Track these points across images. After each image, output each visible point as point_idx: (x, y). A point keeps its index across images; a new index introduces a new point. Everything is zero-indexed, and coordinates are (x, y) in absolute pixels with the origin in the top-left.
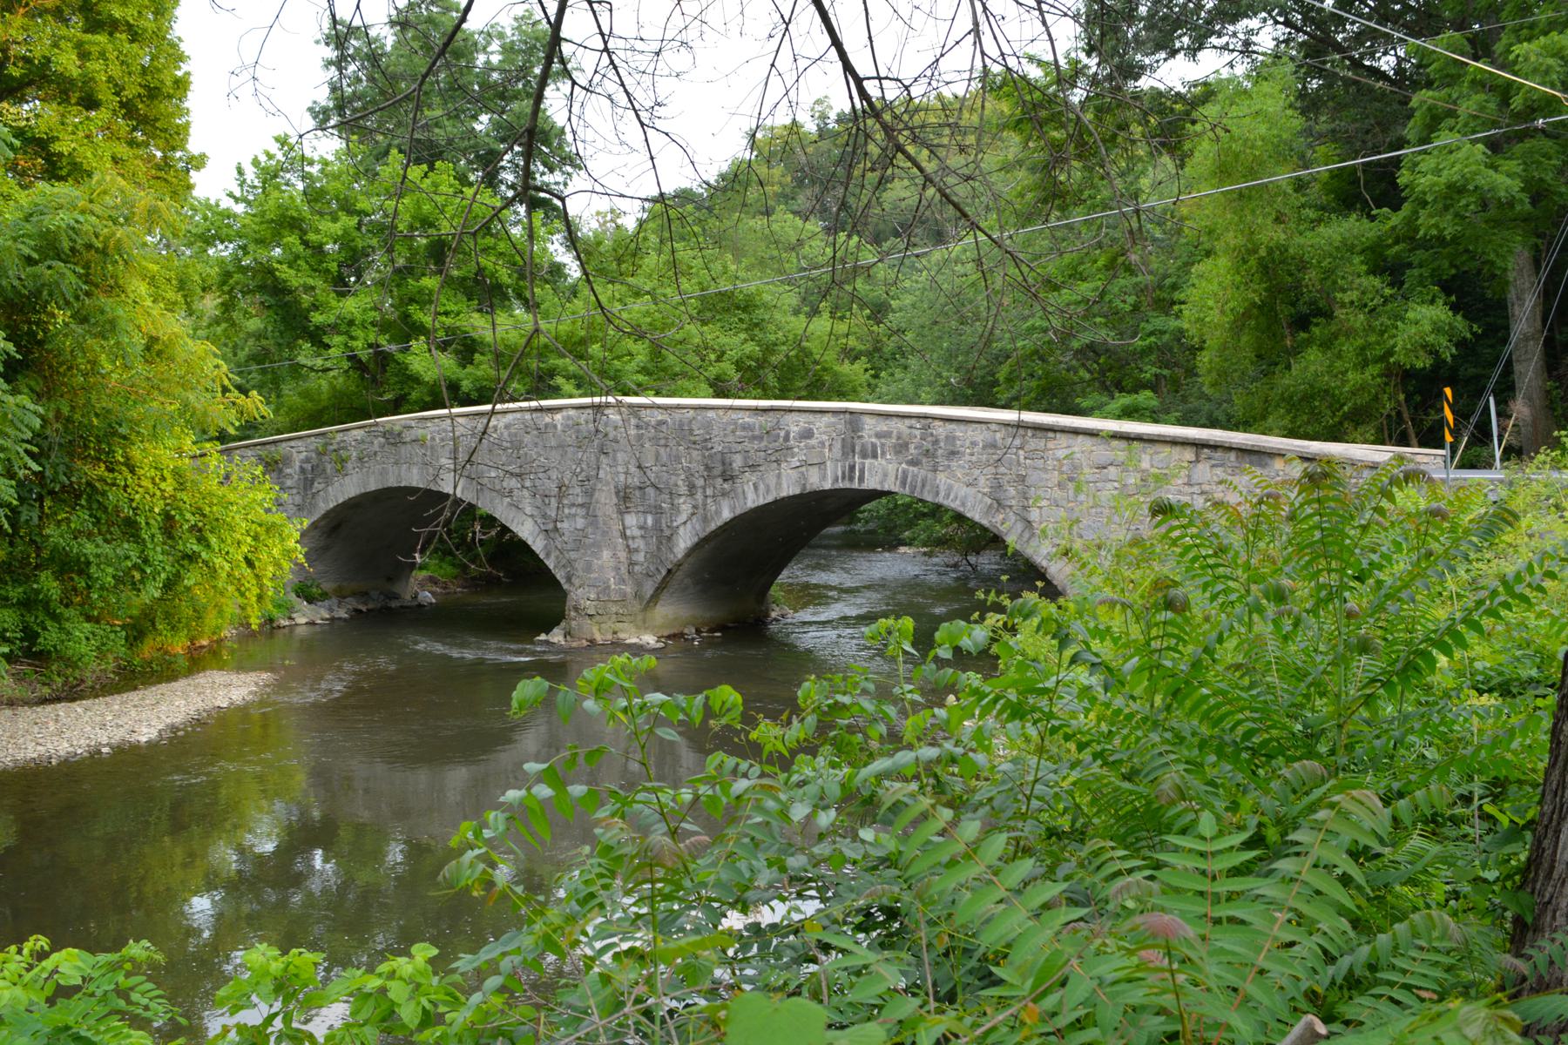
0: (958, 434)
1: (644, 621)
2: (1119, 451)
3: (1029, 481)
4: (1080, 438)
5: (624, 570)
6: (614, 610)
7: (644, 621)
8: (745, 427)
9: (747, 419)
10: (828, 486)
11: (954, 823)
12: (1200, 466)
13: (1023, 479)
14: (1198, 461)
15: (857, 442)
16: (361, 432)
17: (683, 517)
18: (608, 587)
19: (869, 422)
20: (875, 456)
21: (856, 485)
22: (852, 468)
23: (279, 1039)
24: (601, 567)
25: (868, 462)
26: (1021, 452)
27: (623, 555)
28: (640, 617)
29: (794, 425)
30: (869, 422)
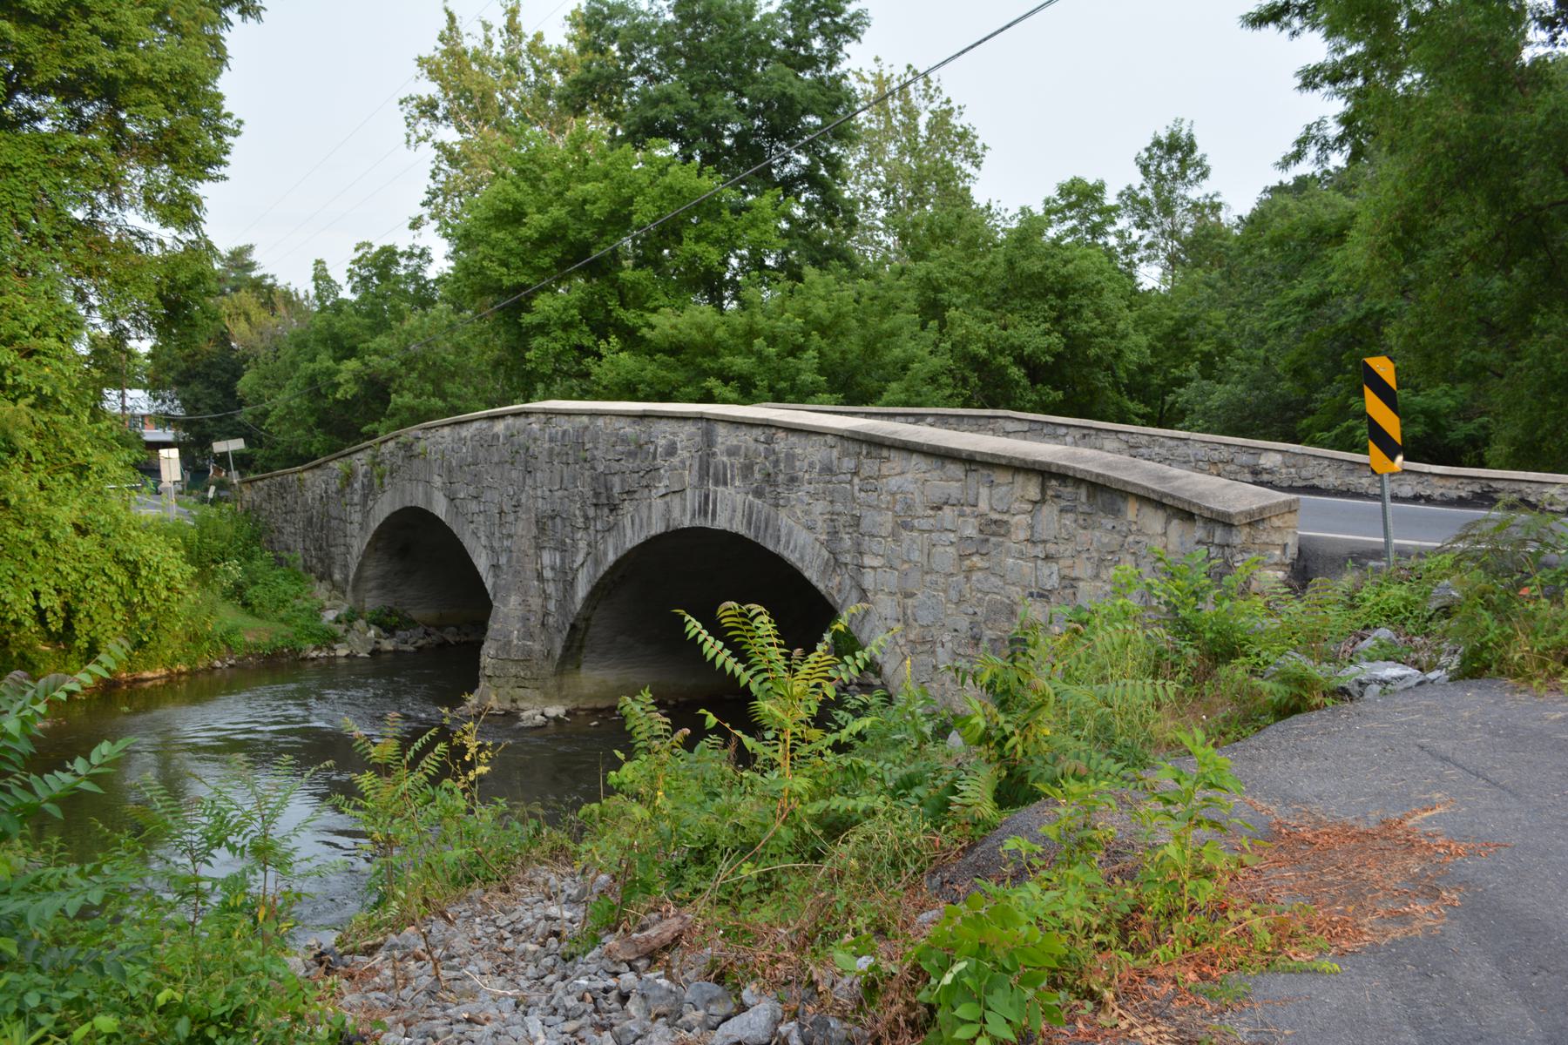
0: (798, 451)
1: (560, 688)
2: (949, 482)
3: (865, 525)
4: (915, 458)
5: (534, 621)
6: (513, 671)
7: (560, 688)
8: (624, 440)
9: (629, 429)
10: (686, 524)
11: (77, 953)
12: (1046, 509)
13: (857, 520)
14: (1043, 501)
15: (712, 460)
16: (1279, 457)
17: (580, 559)
18: (510, 642)
19: (721, 431)
20: (725, 484)
21: (709, 525)
22: (707, 497)
23: (6, 989)
24: (506, 616)
25: (720, 489)
26: (856, 480)
27: (535, 602)
28: (551, 682)
29: (662, 434)
30: (721, 431)
